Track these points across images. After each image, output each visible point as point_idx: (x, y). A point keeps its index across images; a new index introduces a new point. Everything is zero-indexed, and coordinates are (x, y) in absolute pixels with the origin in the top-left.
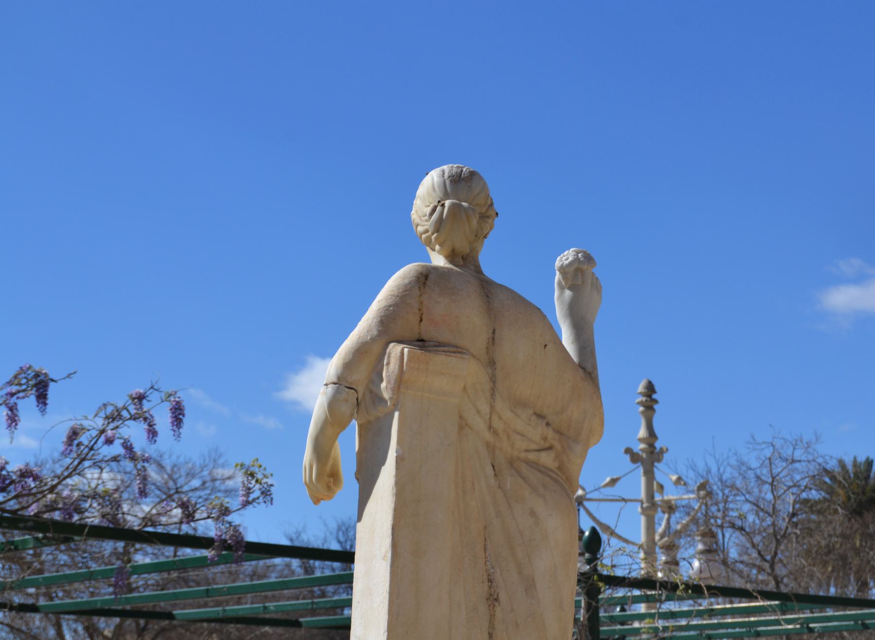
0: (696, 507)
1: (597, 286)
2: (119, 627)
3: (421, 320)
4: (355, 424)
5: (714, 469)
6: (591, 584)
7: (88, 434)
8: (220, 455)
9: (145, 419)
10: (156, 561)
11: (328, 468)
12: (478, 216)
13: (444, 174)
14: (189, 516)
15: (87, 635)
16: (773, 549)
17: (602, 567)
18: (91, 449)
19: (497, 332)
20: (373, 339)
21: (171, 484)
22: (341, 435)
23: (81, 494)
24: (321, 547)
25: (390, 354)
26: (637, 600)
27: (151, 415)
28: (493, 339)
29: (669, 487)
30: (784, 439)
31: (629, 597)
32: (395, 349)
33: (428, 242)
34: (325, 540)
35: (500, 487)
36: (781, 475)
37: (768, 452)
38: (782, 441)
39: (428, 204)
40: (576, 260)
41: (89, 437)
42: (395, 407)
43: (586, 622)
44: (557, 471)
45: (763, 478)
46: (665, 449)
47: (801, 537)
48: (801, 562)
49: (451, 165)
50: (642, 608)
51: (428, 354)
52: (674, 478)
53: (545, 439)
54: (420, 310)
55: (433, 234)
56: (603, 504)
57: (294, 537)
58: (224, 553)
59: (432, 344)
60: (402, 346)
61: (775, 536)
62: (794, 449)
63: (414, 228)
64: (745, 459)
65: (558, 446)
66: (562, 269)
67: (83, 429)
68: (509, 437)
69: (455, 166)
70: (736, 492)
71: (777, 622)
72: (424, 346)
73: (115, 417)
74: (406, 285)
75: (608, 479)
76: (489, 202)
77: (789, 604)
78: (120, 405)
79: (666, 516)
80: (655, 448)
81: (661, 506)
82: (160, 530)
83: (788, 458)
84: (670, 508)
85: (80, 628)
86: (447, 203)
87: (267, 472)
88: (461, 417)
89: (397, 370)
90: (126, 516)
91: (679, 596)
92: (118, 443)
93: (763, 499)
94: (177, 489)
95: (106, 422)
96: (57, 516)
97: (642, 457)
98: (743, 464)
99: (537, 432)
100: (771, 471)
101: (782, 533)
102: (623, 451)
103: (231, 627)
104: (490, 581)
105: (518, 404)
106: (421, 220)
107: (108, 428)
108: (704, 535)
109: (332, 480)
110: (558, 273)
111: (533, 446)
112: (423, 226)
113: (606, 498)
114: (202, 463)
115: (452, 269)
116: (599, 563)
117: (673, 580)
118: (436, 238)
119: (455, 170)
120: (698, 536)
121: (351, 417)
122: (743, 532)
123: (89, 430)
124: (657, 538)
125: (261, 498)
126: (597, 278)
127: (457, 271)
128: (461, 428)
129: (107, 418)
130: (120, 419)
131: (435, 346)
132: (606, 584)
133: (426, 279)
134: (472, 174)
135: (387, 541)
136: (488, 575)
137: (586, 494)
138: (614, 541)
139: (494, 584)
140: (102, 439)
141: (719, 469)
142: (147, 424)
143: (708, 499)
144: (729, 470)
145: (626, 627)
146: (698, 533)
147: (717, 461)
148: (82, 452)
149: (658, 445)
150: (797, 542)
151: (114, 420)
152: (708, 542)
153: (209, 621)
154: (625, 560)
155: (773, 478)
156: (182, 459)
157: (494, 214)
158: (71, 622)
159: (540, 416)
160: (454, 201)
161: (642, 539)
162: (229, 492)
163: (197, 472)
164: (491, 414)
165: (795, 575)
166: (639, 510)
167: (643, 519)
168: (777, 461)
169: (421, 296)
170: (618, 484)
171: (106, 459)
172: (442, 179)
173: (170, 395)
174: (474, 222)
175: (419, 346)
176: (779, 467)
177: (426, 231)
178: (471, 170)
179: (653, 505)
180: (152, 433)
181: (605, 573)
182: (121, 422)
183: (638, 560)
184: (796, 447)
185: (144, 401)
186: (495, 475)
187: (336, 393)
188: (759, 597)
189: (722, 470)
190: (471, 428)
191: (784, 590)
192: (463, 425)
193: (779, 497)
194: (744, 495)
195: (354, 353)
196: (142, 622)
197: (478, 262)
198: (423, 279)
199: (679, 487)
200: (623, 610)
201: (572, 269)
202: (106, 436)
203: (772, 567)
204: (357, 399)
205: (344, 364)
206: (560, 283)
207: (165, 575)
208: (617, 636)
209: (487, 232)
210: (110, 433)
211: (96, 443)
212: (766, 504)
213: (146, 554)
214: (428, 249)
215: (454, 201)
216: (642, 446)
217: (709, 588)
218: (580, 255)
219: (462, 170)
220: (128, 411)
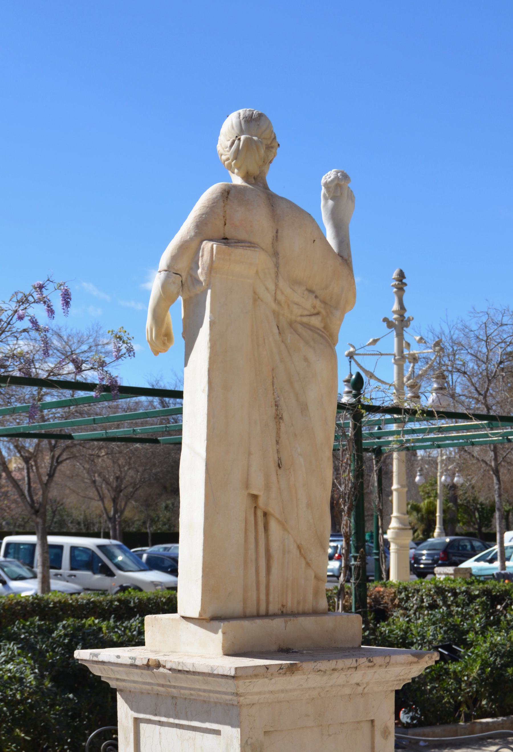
0: (433, 359)
1: (351, 197)
2: (38, 445)
3: (225, 224)
4: (180, 299)
5: (447, 332)
6: (357, 411)
7: (6, 313)
8: (101, 328)
9: (45, 302)
10: (59, 400)
11: (163, 330)
12: (264, 147)
13: (240, 116)
14: (79, 369)
15: (16, 451)
16: (486, 386)
17: (364, 399)
18: (9, 324)
19: (279, 231)
20: (191, 239)
21: (67, 348)
22: (171, 307)
23: (4, 355)
24: (173, 389)
25: (203, 249)
26: (388, 422)
27: (48, 300)
28: (277, 236)
29: (414, 344)
30: (496, 309)
31: (383, 420)
32: (207, 245)
33: (230, 167)
34: (176, 386)
35: (283, 342)
36: (493, 335)
37: (484, 319)
38: (494, 311)
39: (229, 139)
40: (336, 178)
41: (7, 315)
42: (208, 286)
43: (353, 437)
44: (323, 330)
45: (481, 337)
46: (411, 318)
47: (506, 378)
48: (505, 395)
49: (245, 109)
50: (394, 427)
51: (230, 248)
52: (418, 338)
53: (314, 307)
54: (224, 217)
55: (233, 161)
56: (365, 357)
57: (154, 384)
58: (103, 393)
59: (233, 241)
60: (212, 243)
61: (488, 377)
62: (503, 316)
63: (219, 156)
64: (468, 324)
65: (323, 312)
66: (326, 185)
67: (2, 310)
68: (288, 306)
69: (248, 110)
70: (461, 347)
71: (486, 436)
72: (228, 243)
73: (24, 301)
74: (214, 199)
75: (371, 340)
76: (273, 136)
77: (494, 423)
78: (27, 293)
79: (412, 365)
80: (404, 317)
81: (408, 358)
82: (61, 378)
83: (498, 322)
84: (414, 359)
85: (12, 447)
86: (243, 138)
87: (130, 336)
88: (255, 293)
89: (208, 261)
90: (38, 370)
91: (418, 418)
92: (27, 319)
93: (480, 352)
94: (72, 351)
95: (18, 305)
97: (395, 323)
98: (466, 328)
100: (486, 332)
101: (493, 375)
102: (382, 320)
103: (113, 444)
104: (277, 405)
105: (295, 283)
106: (224, 151)
107: (19, 309)
108: (437, 378)
109: (166, 338)
110: (323, 188)
111: (306, 313)
112: (226, 155)
113: (368, 353)
114: (88, 333)
115: (247, 187)
116: (362, 397)
117: (413, 408)
118: (235, 164)
119: (247, 113)
120: (433, 378)
121: (178, 294)
122: (466, 376)
123: (6, 311)
124: (405, 380)
125: (127, 354)
126: (351, 191)
127: (250, 188)
128: (255, 301)
129: (18, 302)
130: (28, 302)
131: (236, 243)
132: (367, 411)
133: (228, 194)
134: (260, 115)
136: (275, 402)
137: (356, 350)
138: (373, 382)
139: (279, 408)
140: (16, 316)
141: (450, 332)
142: (46, 306)
143: (441, 352)
144: (457, 332)
145: (381, 440)
146: (434, 376)
147: (449, 326)
148: (2, 326)
149: (406, 315)
150: (503, 381)
151: (23, 303)
152: (441, 382)
154: (381, 394)
155: (487, 337)
156: (74, 331)
157: (277, 145)
158: (5, 443)
159: (311, 291)
160: (247, 136)
161: (394, 379)
162: (107, 353)
163: (85, 340)
164: (276, 290)
165: (501, 404)
166: (393, 361)
167: (395, 367)
168: (491, 325)
169: (224, 206)
170: (378, 343)
171: (19, 331)
172: (238, 120)
173: (61, 285)
174: (262, 151)
175: (224, 243)
176: (492, 328)
177: (228, 159)
178: (260, 112)
179: (403, 357)
180: (51, 311)
181: (366, 403)
182: (28, 304)
183: (389, 395)
184: (505, 315)
185: (43, 290)
186: (280, 333)
187: (167, 278)
188: (473, 418)
189: (452, 333)
190: (262, 301)
191: (492, 413)
192: (256, 298)
193: (491, 350)
194: (467, 350)
195: (178, 249)
196: (53, 442)
197: (265, 180)
198: (226, 194)
199: (421, 344)
200: (379, 429)
201: (333, 184)
202: (18, 314)
203: (485, 397)
204: (182, 282)
205: (172, 257)
206: (324, 195)
207: (66, 409)
208: (375, 447)
209: (271, 159)
210: (21, 312)
211: (11, 319)
212: (481, 355)
213: (52, 395)
214: (230, 172)
215: (247, 136)
216: (395, 316)
217: (438, 412)
218: (339, 174)
219: (253, 113)
220: (33, 297)
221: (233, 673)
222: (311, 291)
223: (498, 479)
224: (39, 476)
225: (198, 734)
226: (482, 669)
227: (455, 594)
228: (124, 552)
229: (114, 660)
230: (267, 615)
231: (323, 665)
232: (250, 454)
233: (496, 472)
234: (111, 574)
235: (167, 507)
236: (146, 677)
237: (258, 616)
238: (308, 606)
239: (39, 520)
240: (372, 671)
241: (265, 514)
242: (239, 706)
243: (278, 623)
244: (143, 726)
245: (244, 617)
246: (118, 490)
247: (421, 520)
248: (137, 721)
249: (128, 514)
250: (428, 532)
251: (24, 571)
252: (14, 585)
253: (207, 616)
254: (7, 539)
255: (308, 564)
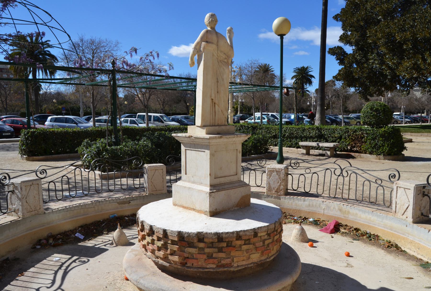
1: (233, 33)
4: (197, 55)
32: (203, 43)
40: (230, 29)
42: (203, 52)
66: (228, 30)
84: (234, 71)
92: (148, 60)
96: (139, 72)
99: (224, 56)
105: (221, 52)
134: (214, 14)
135: (202, 73)
153: (162, 89)
159: (225, 54)
174: (215, 22)
176: (252, 64)
180: (154, 58)
187: (194, 50)
192: (213, 55)
221: (209, 138)
222: (225, 54)
223: (254, 100)
224: (146, 98)
225: (200, 152)
226: (252, 144)
227: (245, 127)
228: (166, 117)
229: (181, 136)
230: (215, 126)
231: (228, 136)
232: (212, 90)
233: (253, 99)
234: (163, 123)
235: (175, 107)
236: (189, 139)
237: (213, 126)
238: (223, 124)
239: (146, 109)
240: (237, 138)
241: (215, 103)
242: (210, 145)
243: (217, 127)
244: (187, 151)
245: (210, 126)
246: (164, 102)
247: (235, 110)
248: (186, 150)
249: (166, 108)
250: (236, 113)
251: (142, 122)
252: (140, 125)
253: (202, 126)
254: (138, 114)
255: (223, 115)
